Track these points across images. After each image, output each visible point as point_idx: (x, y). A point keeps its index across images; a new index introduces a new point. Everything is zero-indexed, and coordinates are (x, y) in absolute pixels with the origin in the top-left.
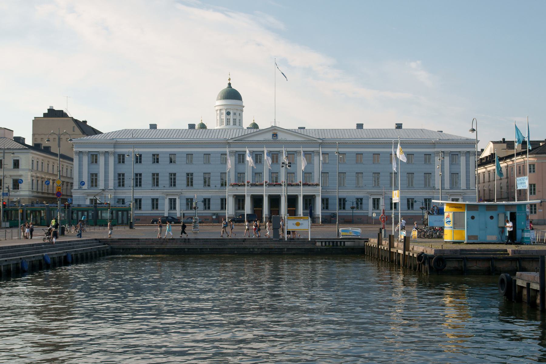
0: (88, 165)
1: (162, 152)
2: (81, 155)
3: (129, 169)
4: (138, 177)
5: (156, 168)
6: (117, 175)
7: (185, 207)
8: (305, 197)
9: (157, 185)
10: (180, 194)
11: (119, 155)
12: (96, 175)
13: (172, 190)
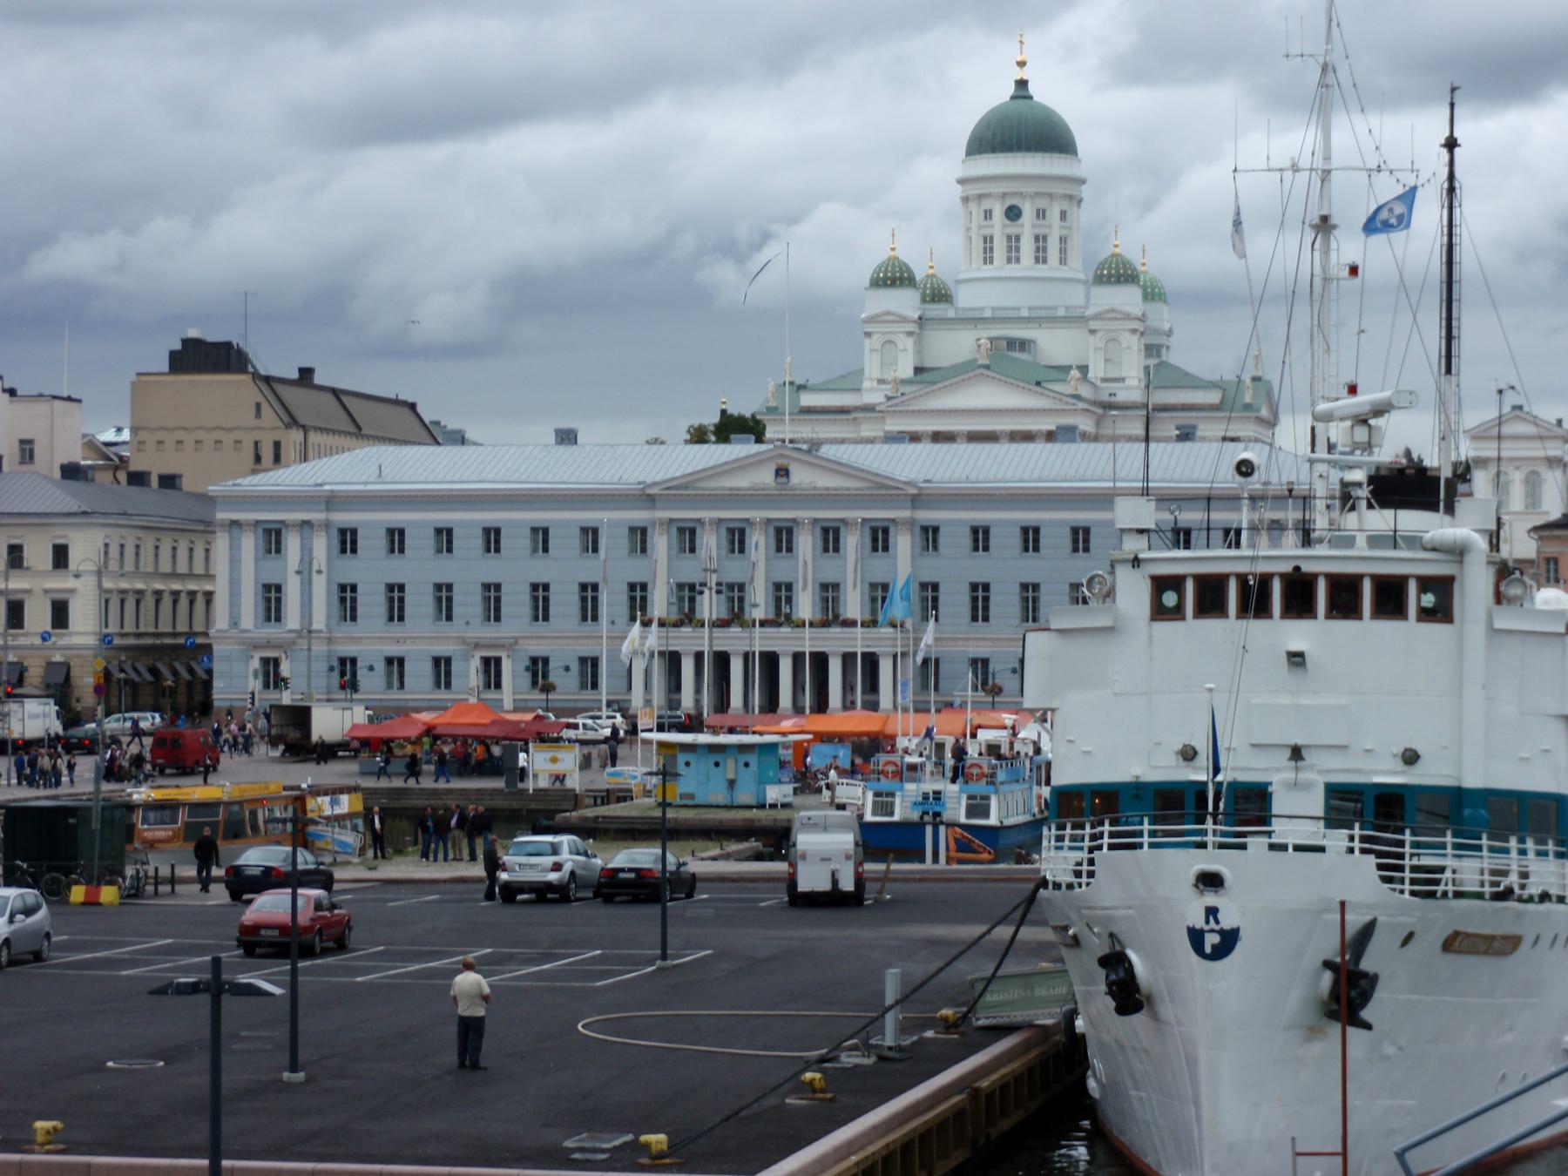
0: (257, 560)
1: (1001, 523)
2: (236, 530)
3: (371, 570)
4: (273, 595)
5: (396, 568)
6: (335, 588)
7: (526, 679)
8: (864, 655)
9: (449, 618)
10: (512, 645)
11: (343, 532)
12: (278, 588)
13: (491, 632)
